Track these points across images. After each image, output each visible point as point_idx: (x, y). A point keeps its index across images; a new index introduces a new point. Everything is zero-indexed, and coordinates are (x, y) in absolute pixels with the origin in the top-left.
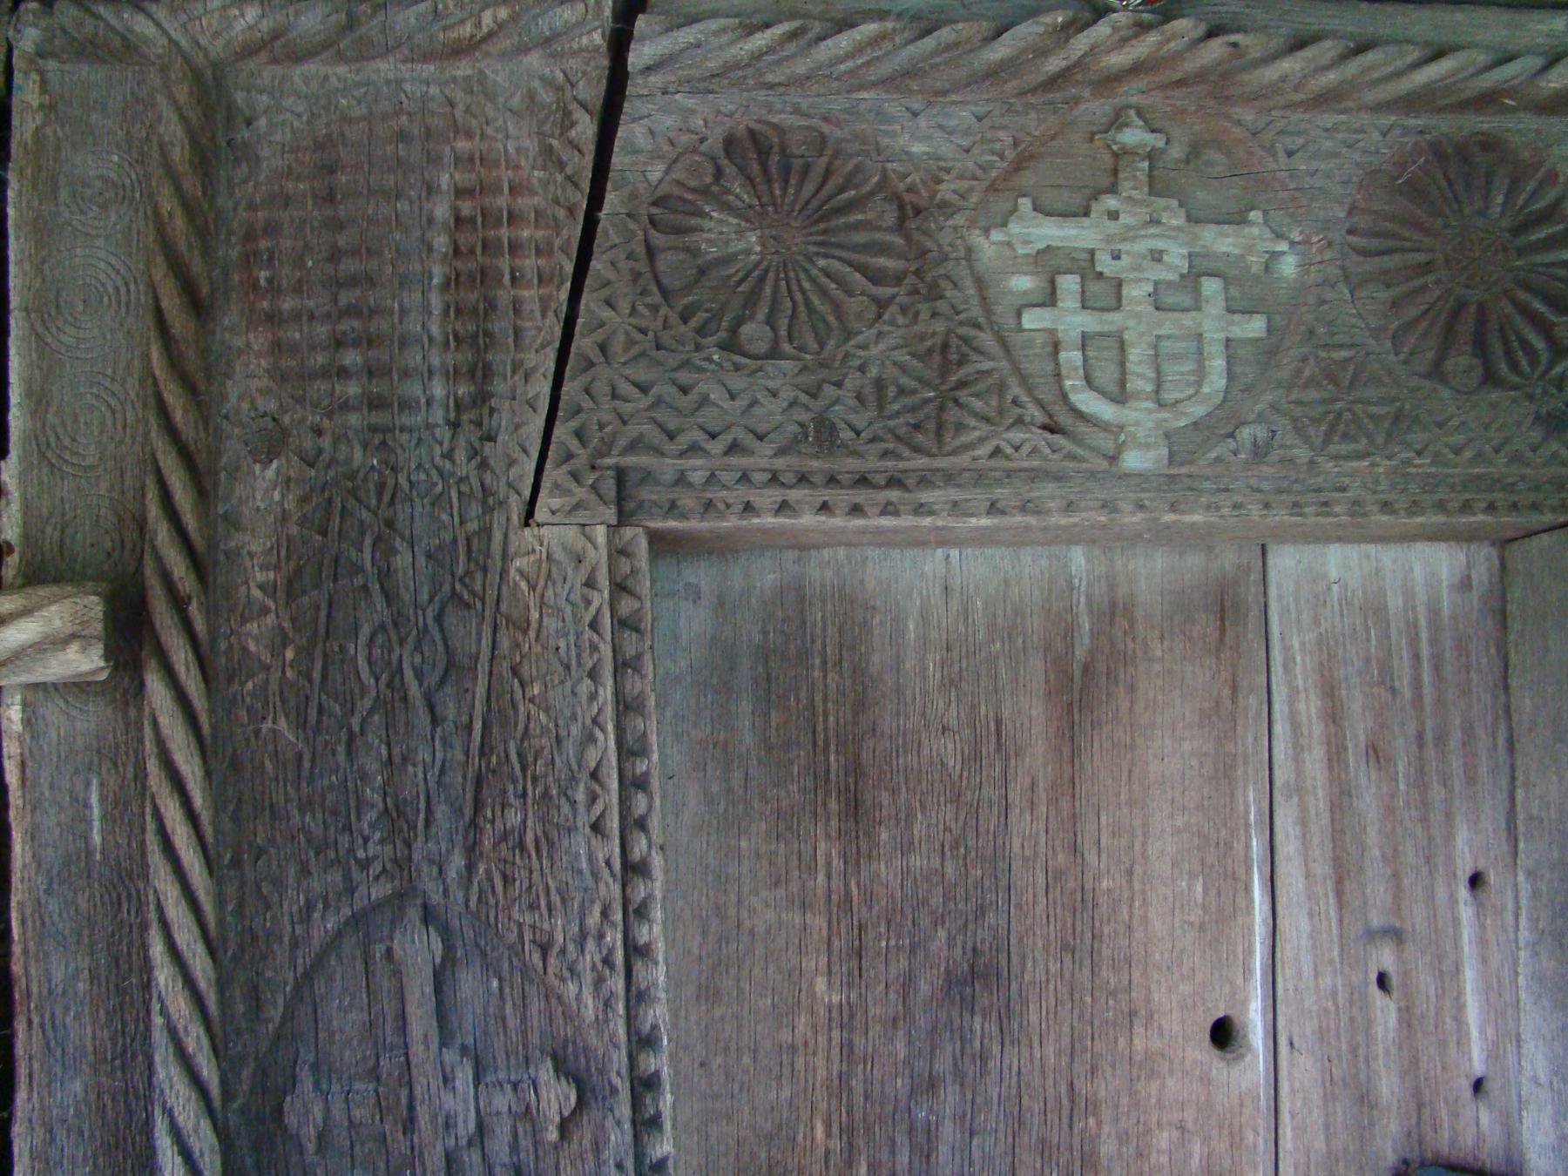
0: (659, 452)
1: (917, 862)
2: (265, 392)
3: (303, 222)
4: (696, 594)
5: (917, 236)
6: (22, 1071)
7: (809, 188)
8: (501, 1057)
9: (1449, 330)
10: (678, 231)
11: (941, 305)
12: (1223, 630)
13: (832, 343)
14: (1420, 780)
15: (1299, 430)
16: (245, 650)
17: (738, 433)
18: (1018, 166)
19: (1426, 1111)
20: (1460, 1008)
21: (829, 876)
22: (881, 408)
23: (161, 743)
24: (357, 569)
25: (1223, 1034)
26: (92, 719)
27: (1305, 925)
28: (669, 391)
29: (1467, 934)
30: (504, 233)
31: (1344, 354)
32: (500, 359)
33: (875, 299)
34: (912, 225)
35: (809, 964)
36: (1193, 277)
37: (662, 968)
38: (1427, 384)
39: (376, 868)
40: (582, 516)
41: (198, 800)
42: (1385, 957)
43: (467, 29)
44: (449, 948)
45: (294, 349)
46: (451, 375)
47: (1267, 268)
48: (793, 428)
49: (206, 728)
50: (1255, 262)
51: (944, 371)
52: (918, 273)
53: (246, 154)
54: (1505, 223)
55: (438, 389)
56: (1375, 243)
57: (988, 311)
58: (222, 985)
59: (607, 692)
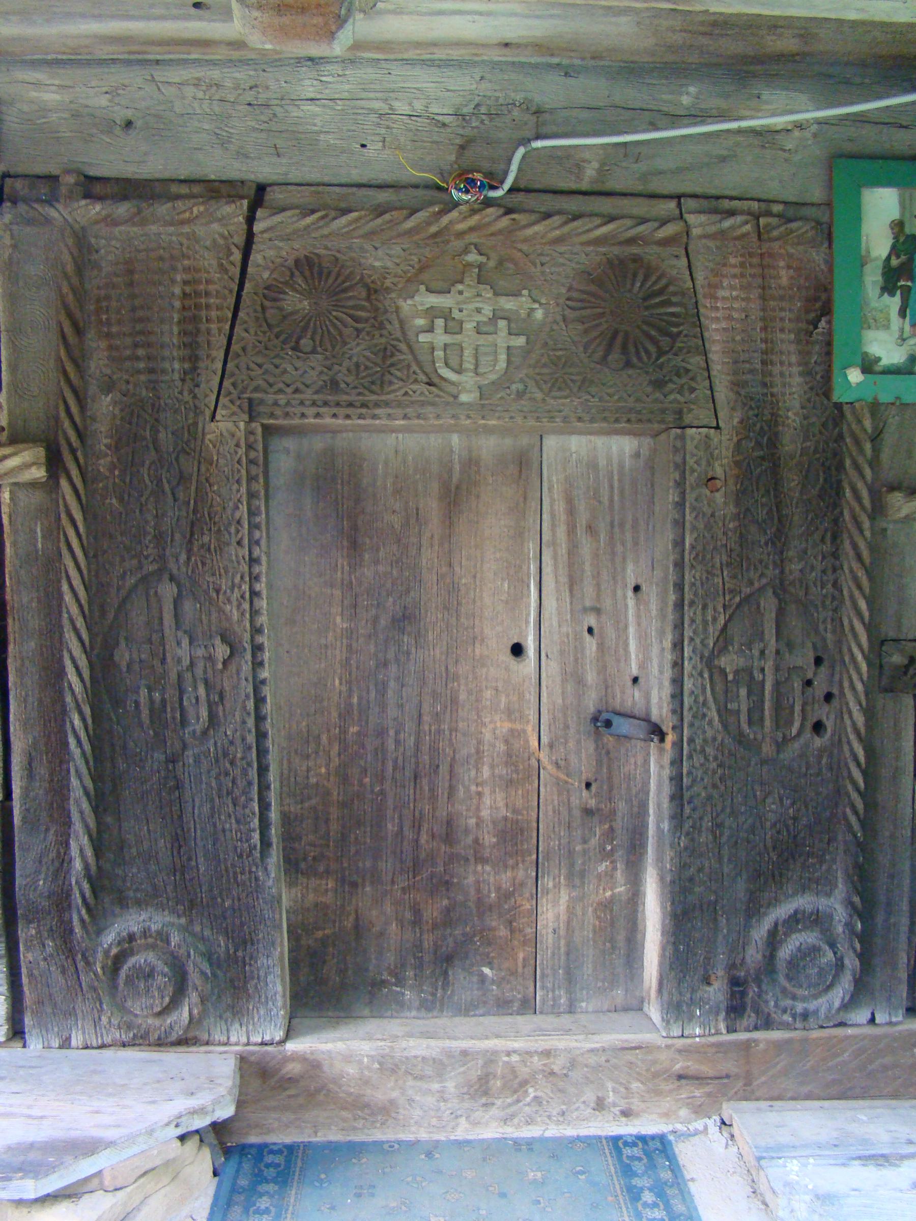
0: (266, 392)
1: (381, 568)
2: (106, 366)
3: (120, 295)
4: (287, 451)
5: (374, 302)
6: (11, 638)
7: (330, 281)
8: (200, 635)
10: (275, 300)
11: (385, 332)
12: (520, 471)
13: (338, 347)
16: (99, 471)
18: (422, 269)
19: (609, 690)
20: (626, 645)
21: (343, 573)
22: (357, 375)
23: (66, 506)
24: (145, 438)
25: (517, 650)
26: (38, 497)
27: (554, 604)
29: (631, 612)
30: (203, 301)
31: (560, 353)
32: (202, 353)
33: (357, 329)
34: (373, 297)
35: (334, 610)
36: (495, 317)
37: (265, 601)
38: (599, 366)
39: (151, 559)
40: (235, 418)
41: (82, 529)
42: (592, 620)
43: (187, 215)
44: (179, 591)
45: (117, 348)
46: (182, 360)
47: (529, 315)
48: (321, 383)
49: (84, 502)
51: (384, 358)
52: (375, 318)
53: (97, 266)
54: (641, 295)
55: (177, 366)
56: (579, 304)
57: (404, 333)
58: (90, 603)
59: (243, 490)
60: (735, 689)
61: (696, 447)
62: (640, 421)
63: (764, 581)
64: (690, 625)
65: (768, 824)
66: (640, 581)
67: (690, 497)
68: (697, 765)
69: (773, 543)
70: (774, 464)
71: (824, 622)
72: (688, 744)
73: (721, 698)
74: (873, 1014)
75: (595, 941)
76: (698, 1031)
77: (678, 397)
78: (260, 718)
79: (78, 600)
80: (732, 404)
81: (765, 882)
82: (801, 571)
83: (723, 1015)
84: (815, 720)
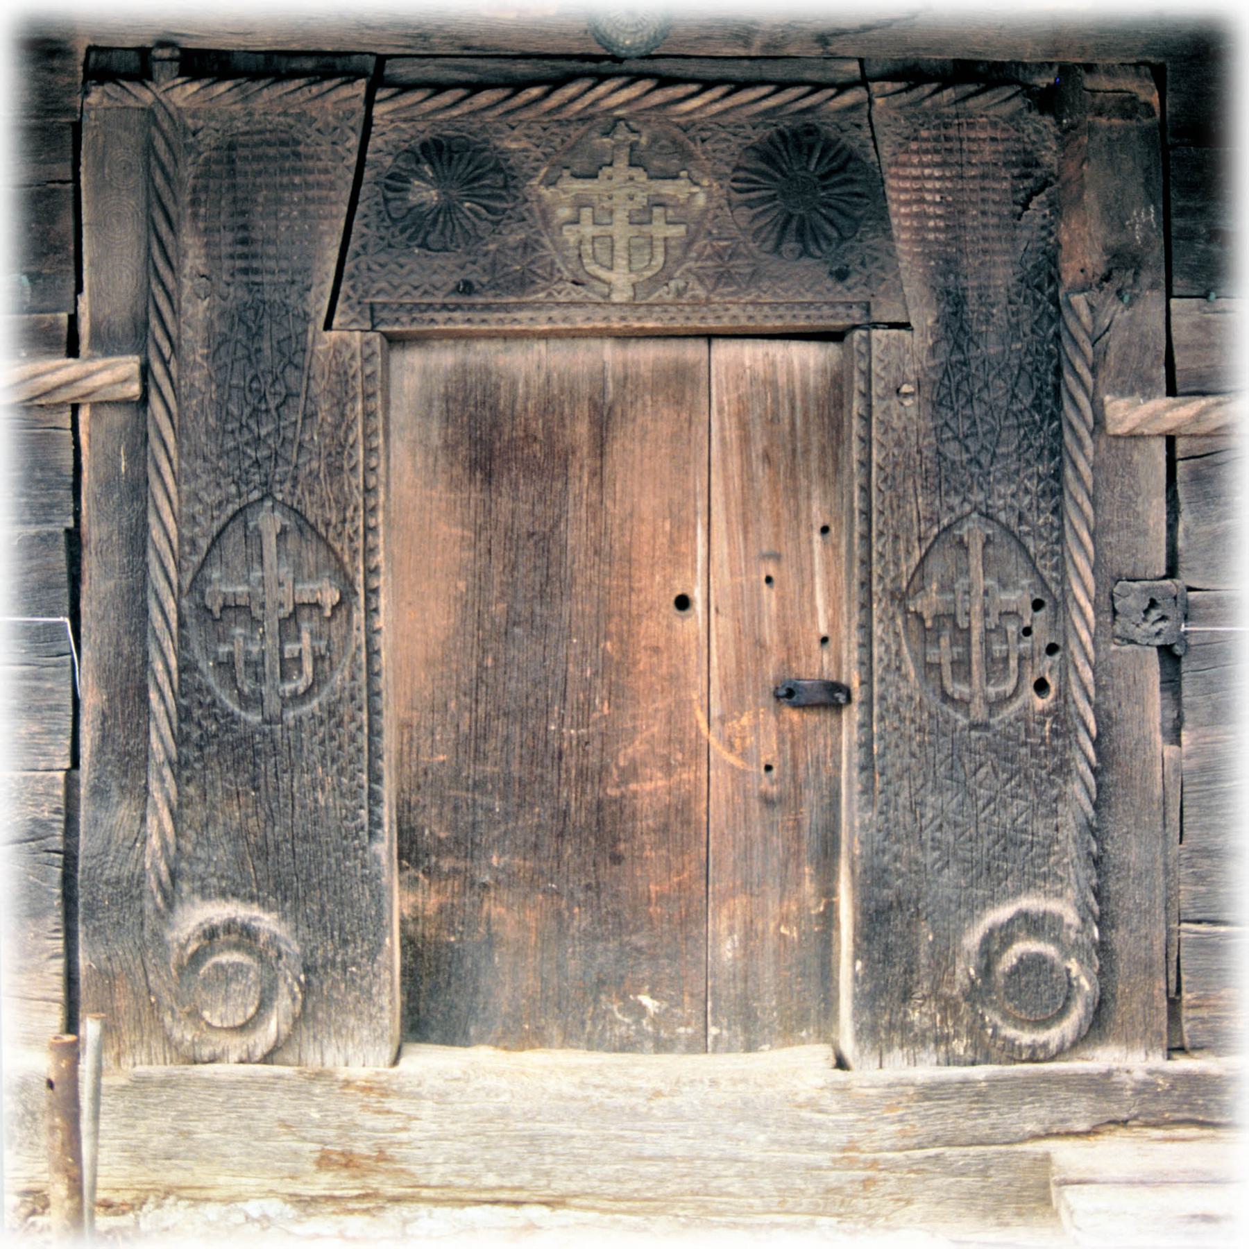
7: (470, 168)
9: (784, 227)
14: (792, 474)
15: (701, 282)
17: (427, 287)
25: (683, 603)
28: (393, 267)
50: (682, 197)
64: (879, 562)
78: (373, 675)
79: (167, 535)
84: (1035, 678)
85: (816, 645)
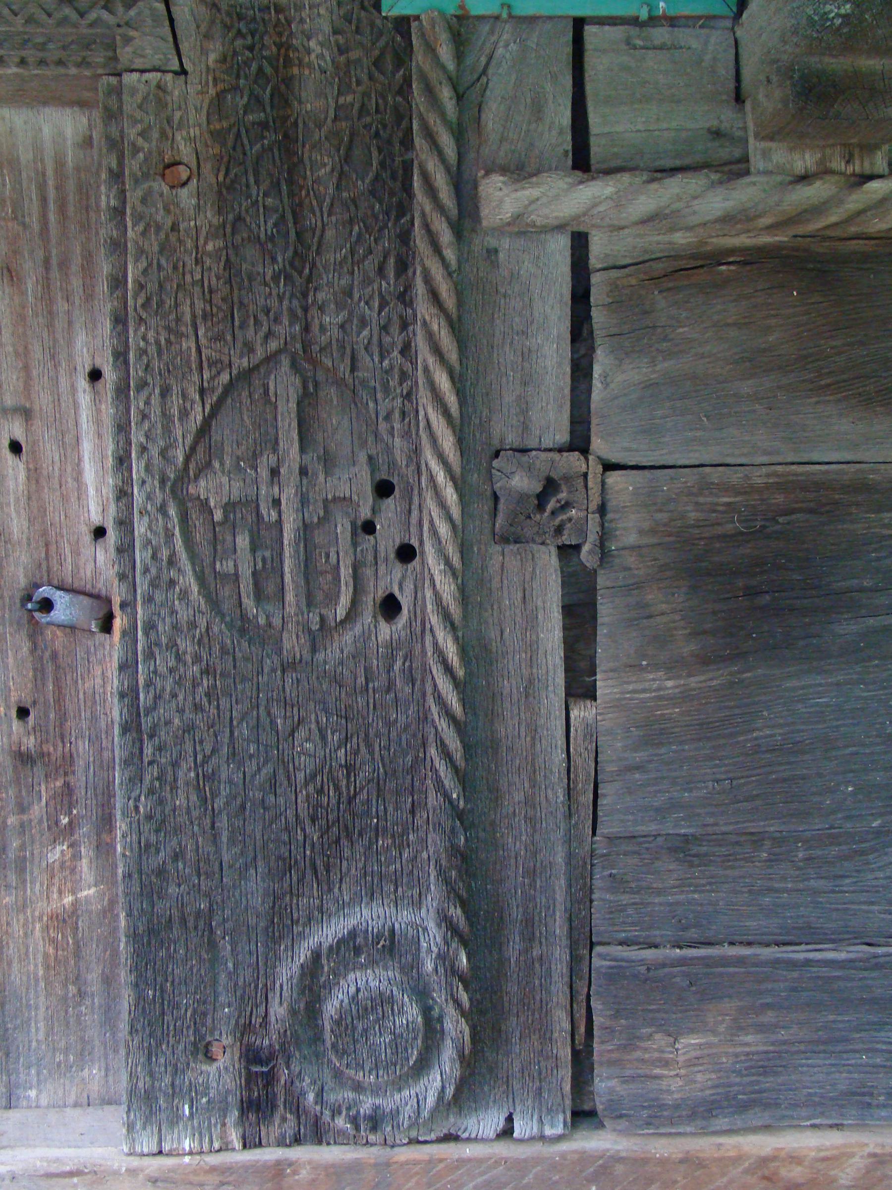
60: (229, 538)
61: (140, 107)
62: (42, 62)
63: (273, 345)
64: (139, 424)
65: (301, 776)
66: (98, 363)
67: (134, 197)
68: (161, 669)
69: (288, 277)
70: (286, 136)
71: (388, 417)
72: (146, 634)
73: (205, 551)
74: (510, 1119)
75: (48, 983)
76: (187, 1145)
77: (105, 15)
80: (203, 28)
81: (301, 880)
82: (342, 327)
83: (234, 1114)
84: (381, 594)
85: (88, 538)
